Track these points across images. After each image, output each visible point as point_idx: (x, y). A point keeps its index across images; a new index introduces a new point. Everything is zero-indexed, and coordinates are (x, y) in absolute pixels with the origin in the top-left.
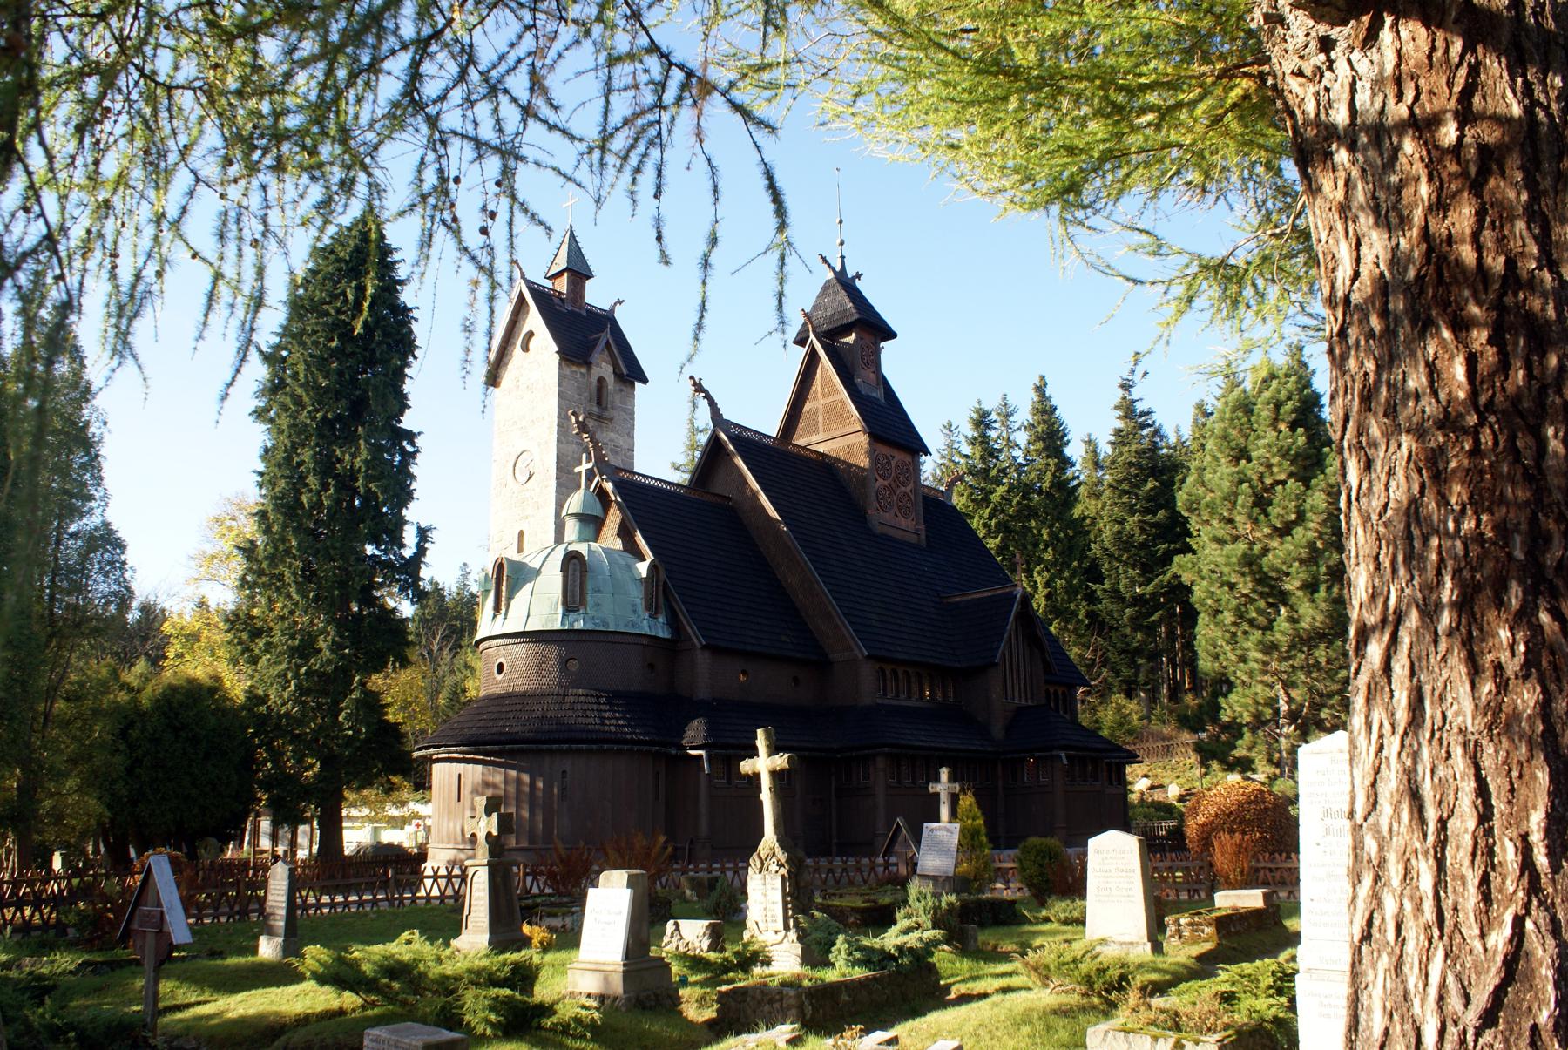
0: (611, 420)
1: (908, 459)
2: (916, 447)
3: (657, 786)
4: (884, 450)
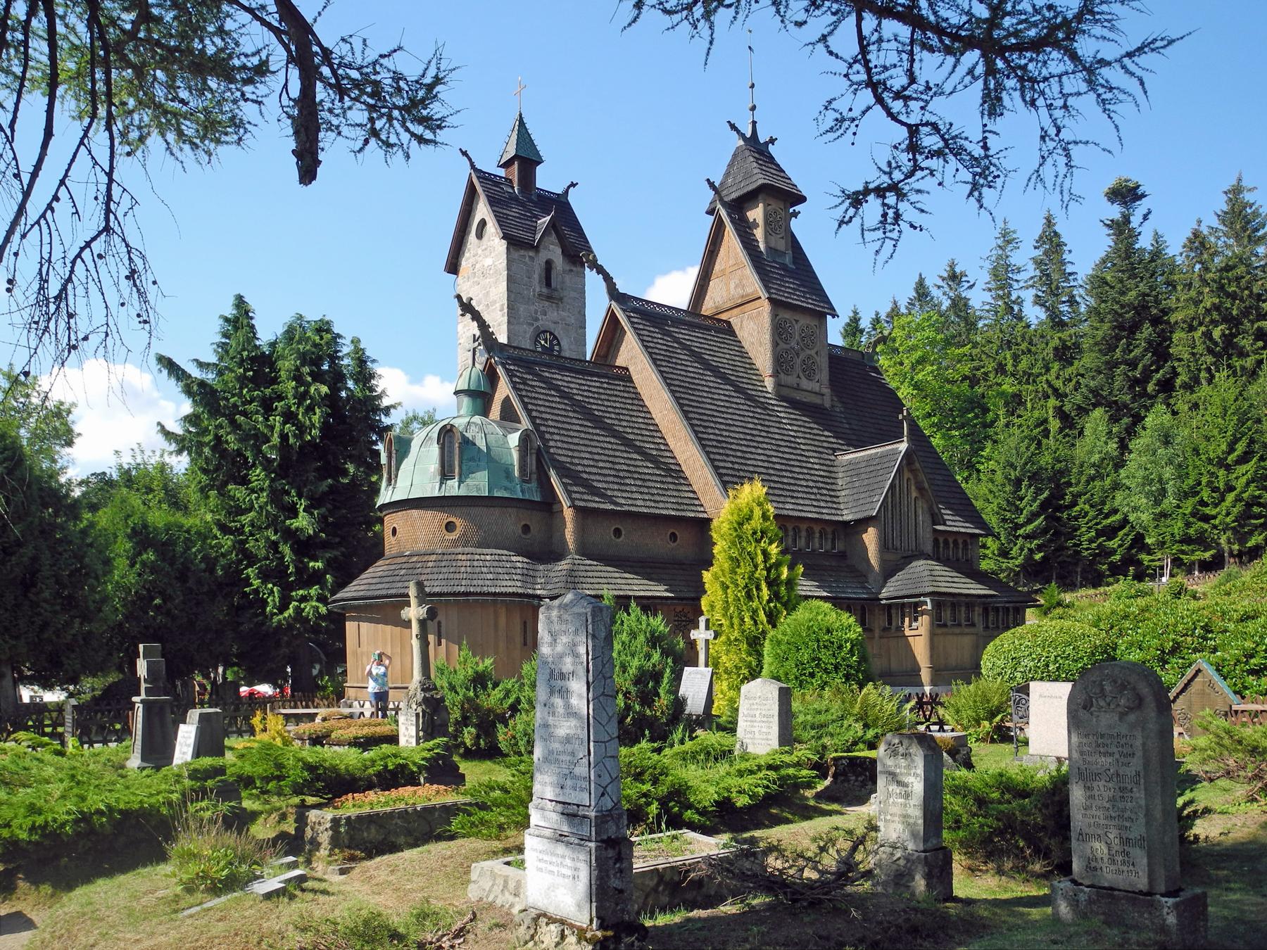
0: (561, 299)
1: (813, 322)
2: (823, 309)
3: (525, 632)
4: (785, 315)
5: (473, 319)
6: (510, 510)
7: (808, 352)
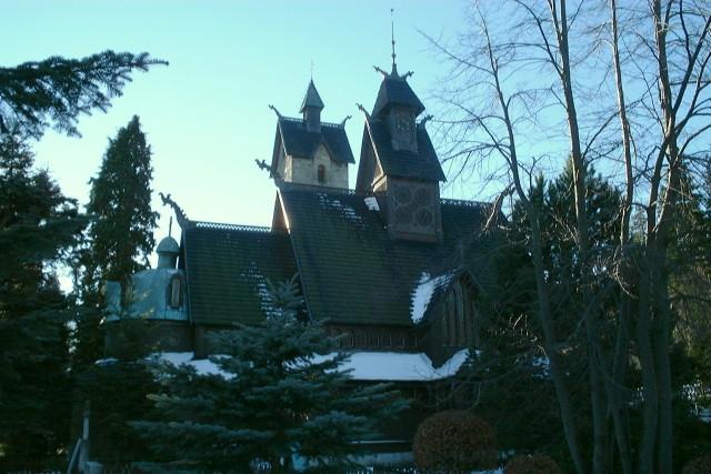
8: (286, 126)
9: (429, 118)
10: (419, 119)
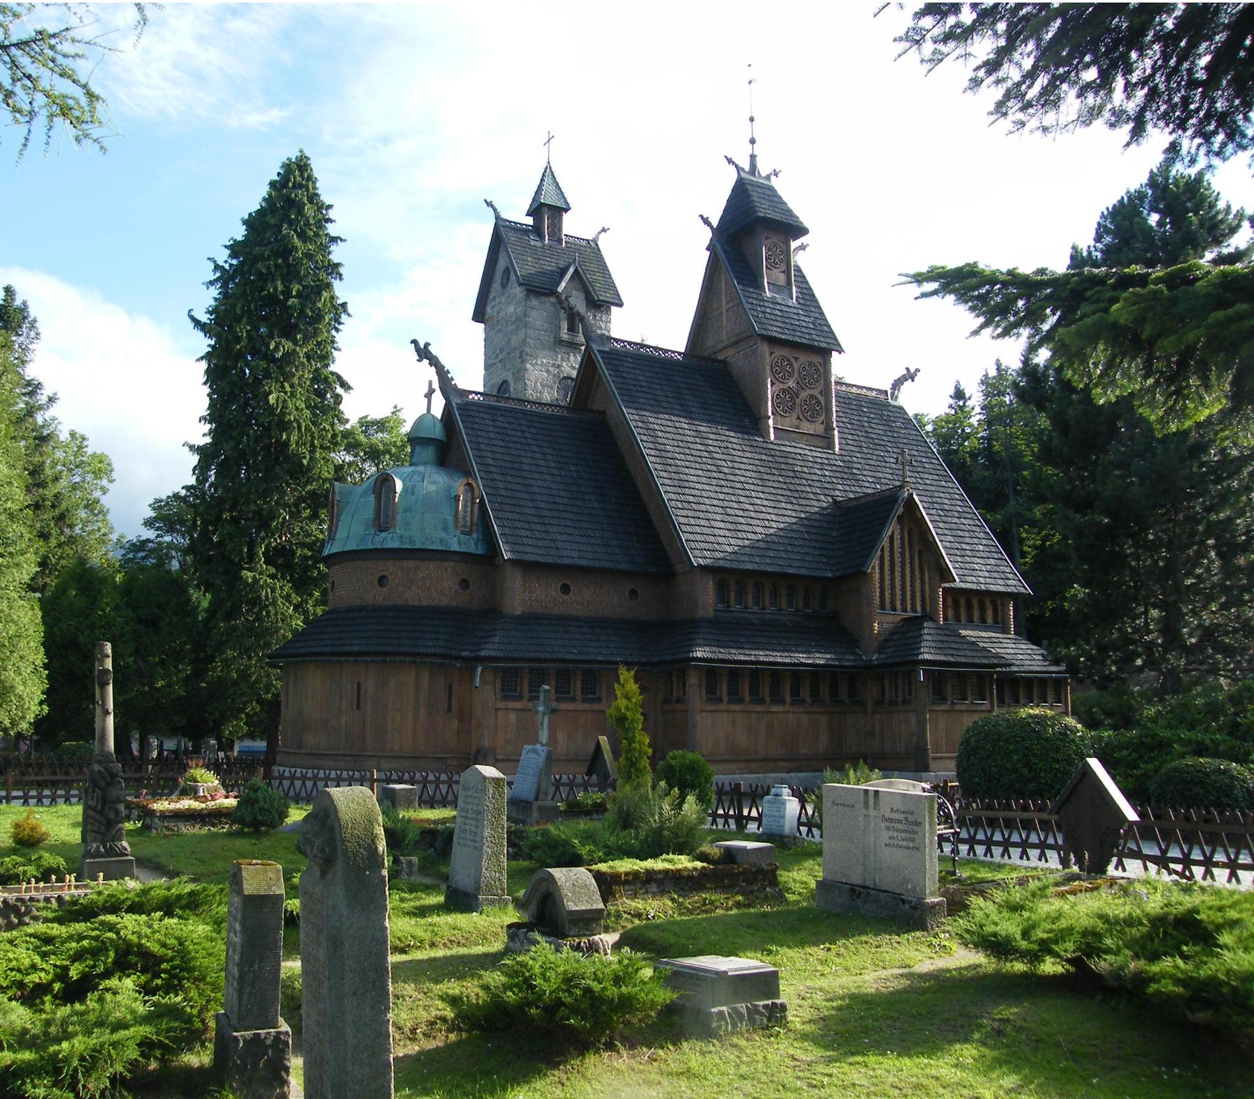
1: (816, 359)
5: (431, 364)
6: (446, 564)
7: (811, 392)
8: (502, 235)
9: (803, 247)
10: (794, 244)
